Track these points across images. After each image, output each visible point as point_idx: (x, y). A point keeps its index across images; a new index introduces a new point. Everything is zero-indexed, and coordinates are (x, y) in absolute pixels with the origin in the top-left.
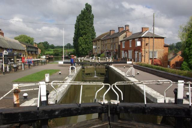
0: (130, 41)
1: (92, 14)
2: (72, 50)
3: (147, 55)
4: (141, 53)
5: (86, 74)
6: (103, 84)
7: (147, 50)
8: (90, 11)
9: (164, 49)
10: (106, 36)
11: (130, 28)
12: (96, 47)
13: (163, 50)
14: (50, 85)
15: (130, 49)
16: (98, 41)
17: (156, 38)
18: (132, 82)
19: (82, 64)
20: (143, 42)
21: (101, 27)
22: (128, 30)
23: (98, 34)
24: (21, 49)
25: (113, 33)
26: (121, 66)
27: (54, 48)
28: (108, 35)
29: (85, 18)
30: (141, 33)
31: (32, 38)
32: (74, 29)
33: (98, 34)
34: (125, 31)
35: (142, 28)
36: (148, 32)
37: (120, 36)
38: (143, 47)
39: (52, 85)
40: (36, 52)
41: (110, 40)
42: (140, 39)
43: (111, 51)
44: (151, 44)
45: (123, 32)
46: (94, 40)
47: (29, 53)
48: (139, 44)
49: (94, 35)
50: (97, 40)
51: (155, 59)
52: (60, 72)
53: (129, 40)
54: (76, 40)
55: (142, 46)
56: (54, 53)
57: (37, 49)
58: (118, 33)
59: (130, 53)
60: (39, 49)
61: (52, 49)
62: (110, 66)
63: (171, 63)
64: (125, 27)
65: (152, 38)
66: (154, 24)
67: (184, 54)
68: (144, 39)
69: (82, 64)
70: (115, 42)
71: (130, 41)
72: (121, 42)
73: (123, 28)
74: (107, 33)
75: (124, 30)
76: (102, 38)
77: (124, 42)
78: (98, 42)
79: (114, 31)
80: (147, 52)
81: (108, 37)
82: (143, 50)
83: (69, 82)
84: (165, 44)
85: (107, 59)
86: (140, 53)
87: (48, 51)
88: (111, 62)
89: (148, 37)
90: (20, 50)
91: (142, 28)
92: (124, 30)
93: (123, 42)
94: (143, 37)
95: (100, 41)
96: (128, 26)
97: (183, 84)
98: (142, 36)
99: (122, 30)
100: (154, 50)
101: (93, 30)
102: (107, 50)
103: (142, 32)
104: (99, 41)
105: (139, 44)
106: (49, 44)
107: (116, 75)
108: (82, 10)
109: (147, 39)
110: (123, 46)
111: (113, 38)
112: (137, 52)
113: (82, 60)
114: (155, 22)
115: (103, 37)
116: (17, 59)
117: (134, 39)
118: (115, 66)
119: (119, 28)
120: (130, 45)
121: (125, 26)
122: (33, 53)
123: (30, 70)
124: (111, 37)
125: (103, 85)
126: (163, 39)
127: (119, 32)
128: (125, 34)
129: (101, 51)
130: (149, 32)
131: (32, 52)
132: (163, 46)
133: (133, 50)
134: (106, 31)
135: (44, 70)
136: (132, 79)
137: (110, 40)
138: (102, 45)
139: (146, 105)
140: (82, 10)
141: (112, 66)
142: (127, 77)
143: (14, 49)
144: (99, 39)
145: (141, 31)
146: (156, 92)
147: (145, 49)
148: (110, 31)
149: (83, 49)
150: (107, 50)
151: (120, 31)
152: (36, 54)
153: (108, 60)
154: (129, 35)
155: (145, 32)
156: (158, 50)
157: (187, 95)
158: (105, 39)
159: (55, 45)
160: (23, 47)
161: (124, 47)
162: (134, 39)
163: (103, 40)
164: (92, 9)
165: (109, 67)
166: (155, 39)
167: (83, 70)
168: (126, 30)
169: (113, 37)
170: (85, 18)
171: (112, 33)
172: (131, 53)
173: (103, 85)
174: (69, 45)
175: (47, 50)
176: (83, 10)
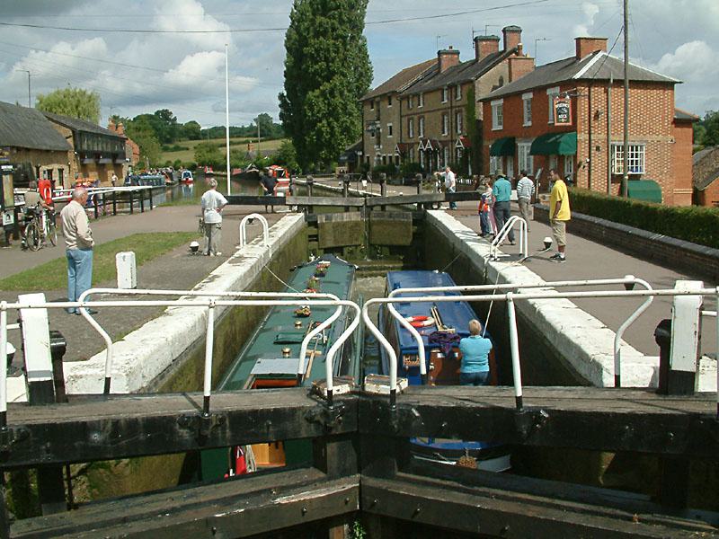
0: (526, 97)
2: (274, 146)
3: (599, 160)
6: (338, 301)
7: (599, 136)
11: (526, 43)
13: (670, 137)
14: (76, 312)
15: (526, 134)
16: (386, 102)
18: (514, 290)
20: (583, 104)
22: (517, 51)
24: (48, 144)
27: (197, 138)
28: (432, 70)
30: (575, 62)
32: (283, 53)
38: (582, 126)
39: (83, 311)
40: (114, 156)
41: (439, 94)
43: (444, 143)
45: (496, 58)
47: (87, 161)
49: (365, 74)
51: (634, 178)
52: (194, 244)
53: (520, 93)
54: (293, 102)
57: (123, 140)
60: (129, 143)
61: (191, 139)
63: (707, 194)
64: (501, 36)
65: (619, 83)
67: (549, 136)
68: (584, 90)
69: (309, 209)
70: (458, 104)
71: (527, 97)
72: (486, 101)
74: (429, 63)
75: (501, 48)
77: (501, 102)
78: (385, 105)
80: (598, 149)
83: (225, 285)
84: (677, 112)
87: (177, 149)
89: (604, 83)
90: (48, 151)
92: (501, 48)
93: (492, 103)
94: (582, 81)
95: (394, 100)
96: (518, 31)
97: (44, 313)
98: (577, 76)
99: (492, 51)
100: (630, 137)
102: (425, 143)
103: (578, 57)
104: (390, 99)
109: (598, 92)
110: (501, 121)
111: (450, 87)
114: (629, 11)
116: (17, 191)
117: (540, 91)
119: (476, 40)
120: (526, 115)
121: (504, 31)
122: (101, 162)
124: (444, 81)
125: (335, 307)
126: (668, 92)
127: (477, 60)
128: (502, 67)
129: (401, 145)
131: (96, 155)
137: (439, 94)
138: (405, 120)
139: (519, 400)
141: (440, 215)
142: (493, 264)
143: (19, 149)
144: (387, 95)
146: (610, 332)
147: (590, 134)
148: (439, 53)
150: (425, 143)
151: (483, 56)
152: (118, 168)
155: (591, 58)
156: (648, 138)
157: (326, 473)
158: (415, 90)
161: (501, 128)
162: (540, 91)
163: (407, 97)
165: (425, 215)
167: (313, 231)
168: (509, 49)
173: (335, 307)
174: (264, 120)
175: (171, 146)
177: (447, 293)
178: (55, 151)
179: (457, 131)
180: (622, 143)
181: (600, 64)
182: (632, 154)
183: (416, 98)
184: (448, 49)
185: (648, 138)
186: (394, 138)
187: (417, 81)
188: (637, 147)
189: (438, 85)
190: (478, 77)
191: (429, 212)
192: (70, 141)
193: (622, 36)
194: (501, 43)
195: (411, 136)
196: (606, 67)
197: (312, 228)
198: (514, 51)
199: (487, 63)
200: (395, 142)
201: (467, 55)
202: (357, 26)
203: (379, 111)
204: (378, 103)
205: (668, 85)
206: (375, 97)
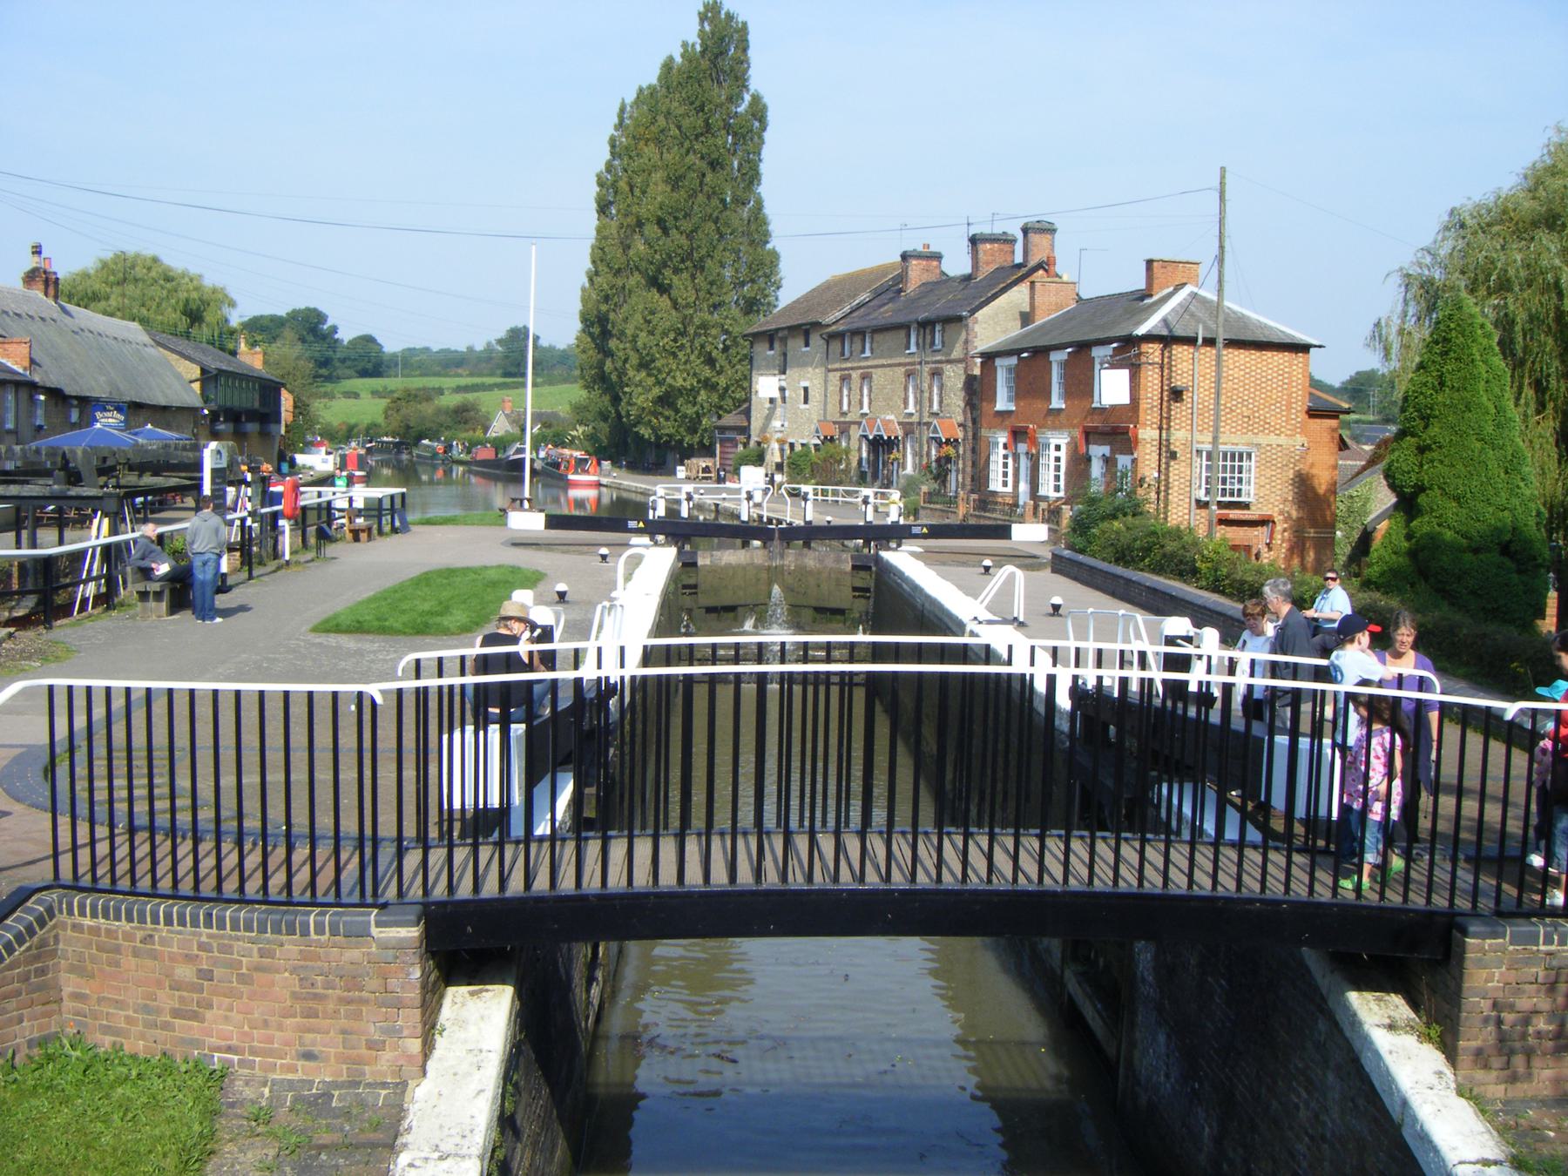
1: (756, 99)
4: (1134, 461)
5: (709, 610)
8: (738, 75)
9: (1304, 432)
10: (864, 297)
12: (782, 389)
13: (1300, 439)
17: (1233, 343)
19: (676, 530)
20: (1151, 380)
21: (823, 219)
22: (1045, 266)
23: (795, 283)
25: (926, 278)
26: (963, 558)
28: (890, 286)
29: (691, 147)
30: (1139, 300)
31: (214, 291)
33: (795, 283)
34: (1019, 266)
35: (1150, 263)
36: (1194, 296)
37: (979, 314)
42: (1128, 350)
44: (1200, 394)
45: (1020, 273)
46: (761, 323)
48: (1113, 387)
49: (764, 268)
50: (793, 330)
52: (561, 587)
55: (1144, 405)
56: (429, 435)
58: (967, 279)
59: (1053, 453)
61: (364, 373)
62: (885, 555)
64: (1020, 236)
66: (1222, 247)
69: (676, 530)
71: (1057, 357)
72: (989, 358)
73: (1008, 240)
76: (839, 314)
77: (1013, 361)
79: (938, 257)
81: (886, 314)
82: (1147, 434)
85: (866, 502)
86: (1123, 461)
88: (895, 525)
90: (165, 408)
91: (1150, 263)
92: (1019, 259)
93: (998, 362)
94: (1149, 338)
95: (816, 340)
96: (1049, 230)
98: (1141, 330)
101: (757, 229)
105: (1113, 387)
106: (334, 329)
107: (923, 615)
108: (671, 59)
112: (1105, 450)
113: (678, 502)
115: (840, 303)
117: (1083, 347)
118: (927, 557)
123: (332, 569)
128: (1018, 296)
130: (1194, 296)
132: (1301, 404)
133: (1077, 433)
134: (877, 253)
135: (390, 582)
136: (998, 637)
137: (903, 333)
140: (671, 59)
141: (903, 559)
145: (1142, 286)
148: (905, 257)
149: (666, 400)
151: (985, 270)
152: (265, 435)
153: (1202, 293)
154: (1051, 304)
156: (1262, 440)
158: (857, 322)
159: (391, 345)
160: (179, 376)
162: (1083, 347)
163: (840, 336)
164: (768, 189)
165: (878, 560)
166: (1238, 360)
168: (1032, 263)
169: (922, 316)
170: (691, 147)
171: (917, 275)
172: (1063, 454)
176: (678, 60)
177: (878, 653)
178: (179, 408)
179: (931, 406)
180: (1209, 447)
181: (1185, 308)
182: (1225, 467)
183: (857, 340)
184: (920, 248)
185: (1262, 440)
186: (814, 409)
187: (859, 307)
188: (1241, 455)
189: (901, 319)
190: (973, 312)
191: (883, 554)
192: (197, 386)
193: (1215, 271)
194: (1019, 248)
195: (845, 408)
196: (1192, 315)
197: (862, 574)
198: (1040, 266)
199: (992, 286)
200: (815, 417)
201: (957, 263)
202: (752, 175)
203: (785, 355)
204: (784, 341)
205: (1304, 348)
206: (777, 330)
